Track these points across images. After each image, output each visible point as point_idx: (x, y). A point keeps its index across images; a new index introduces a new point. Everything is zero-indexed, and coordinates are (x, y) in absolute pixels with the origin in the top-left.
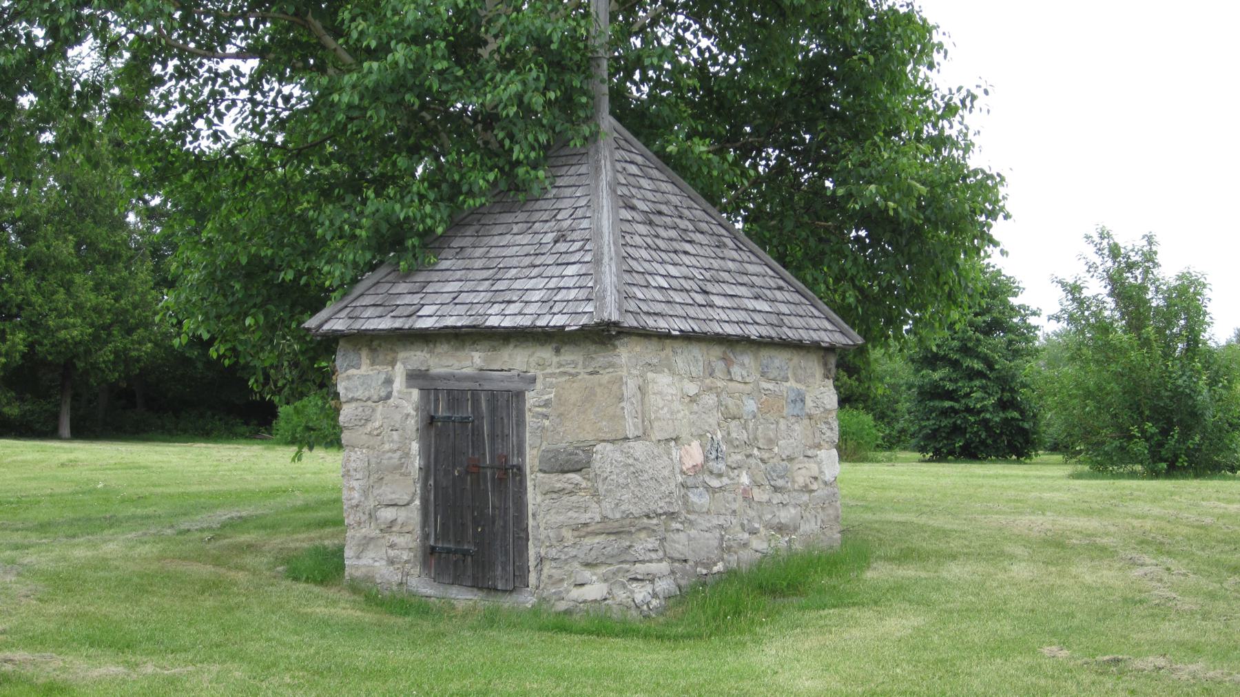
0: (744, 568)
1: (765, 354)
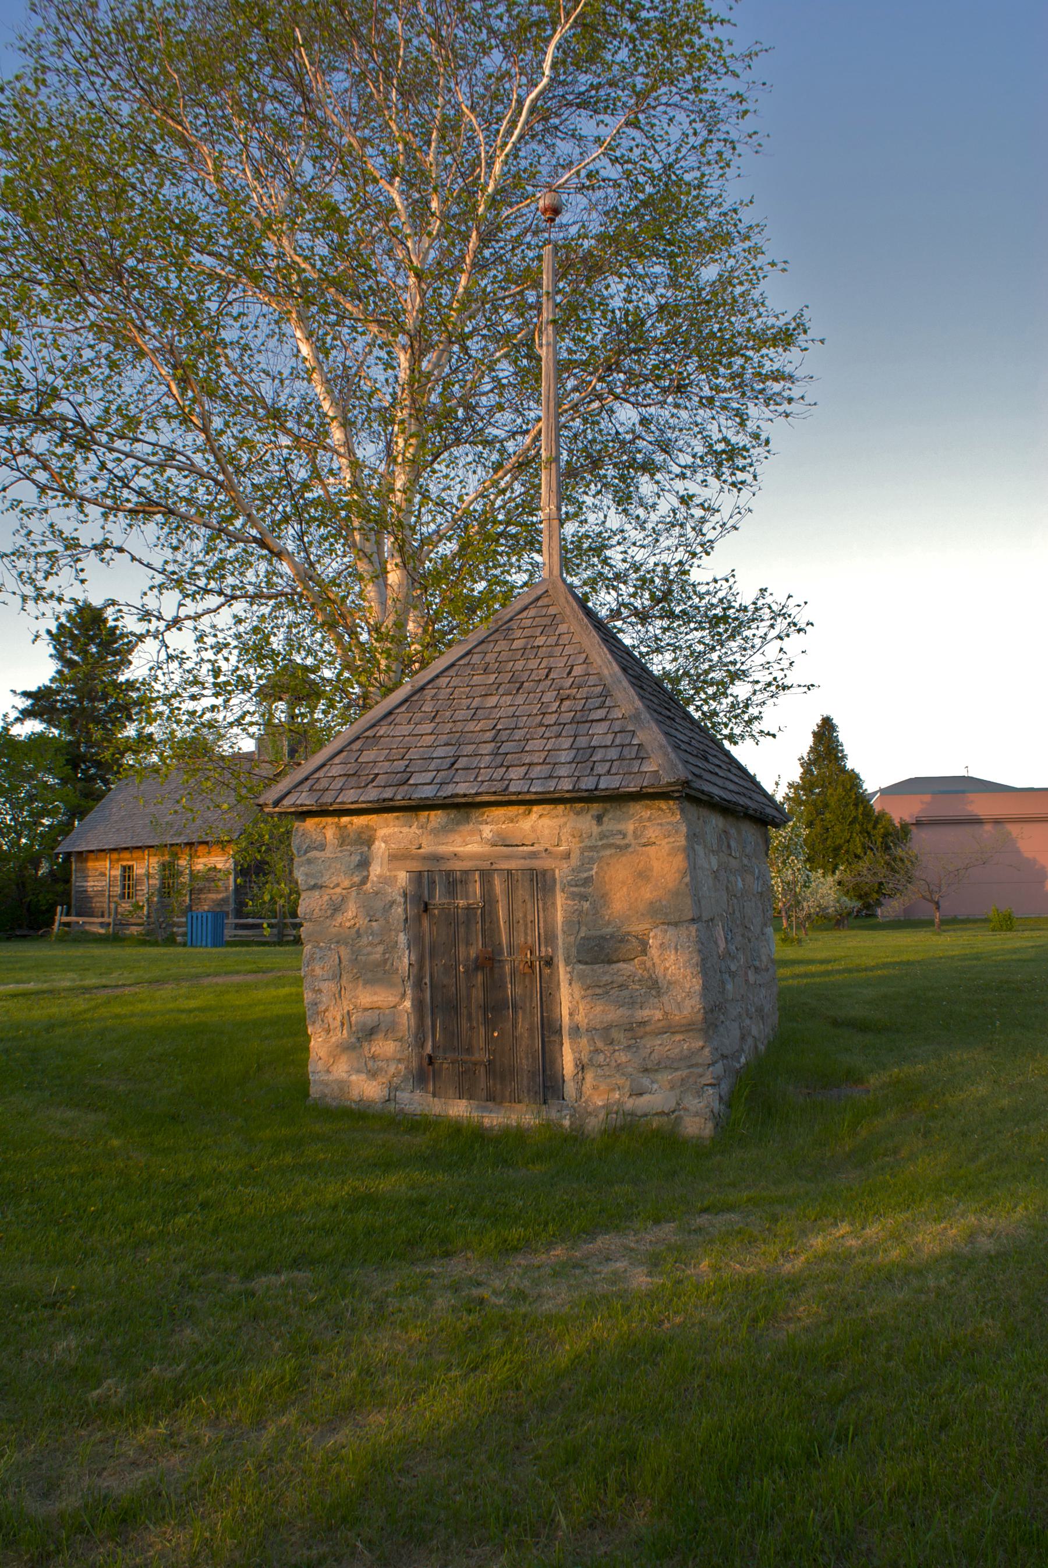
0: (593, 1124)
1: (704, 812)
